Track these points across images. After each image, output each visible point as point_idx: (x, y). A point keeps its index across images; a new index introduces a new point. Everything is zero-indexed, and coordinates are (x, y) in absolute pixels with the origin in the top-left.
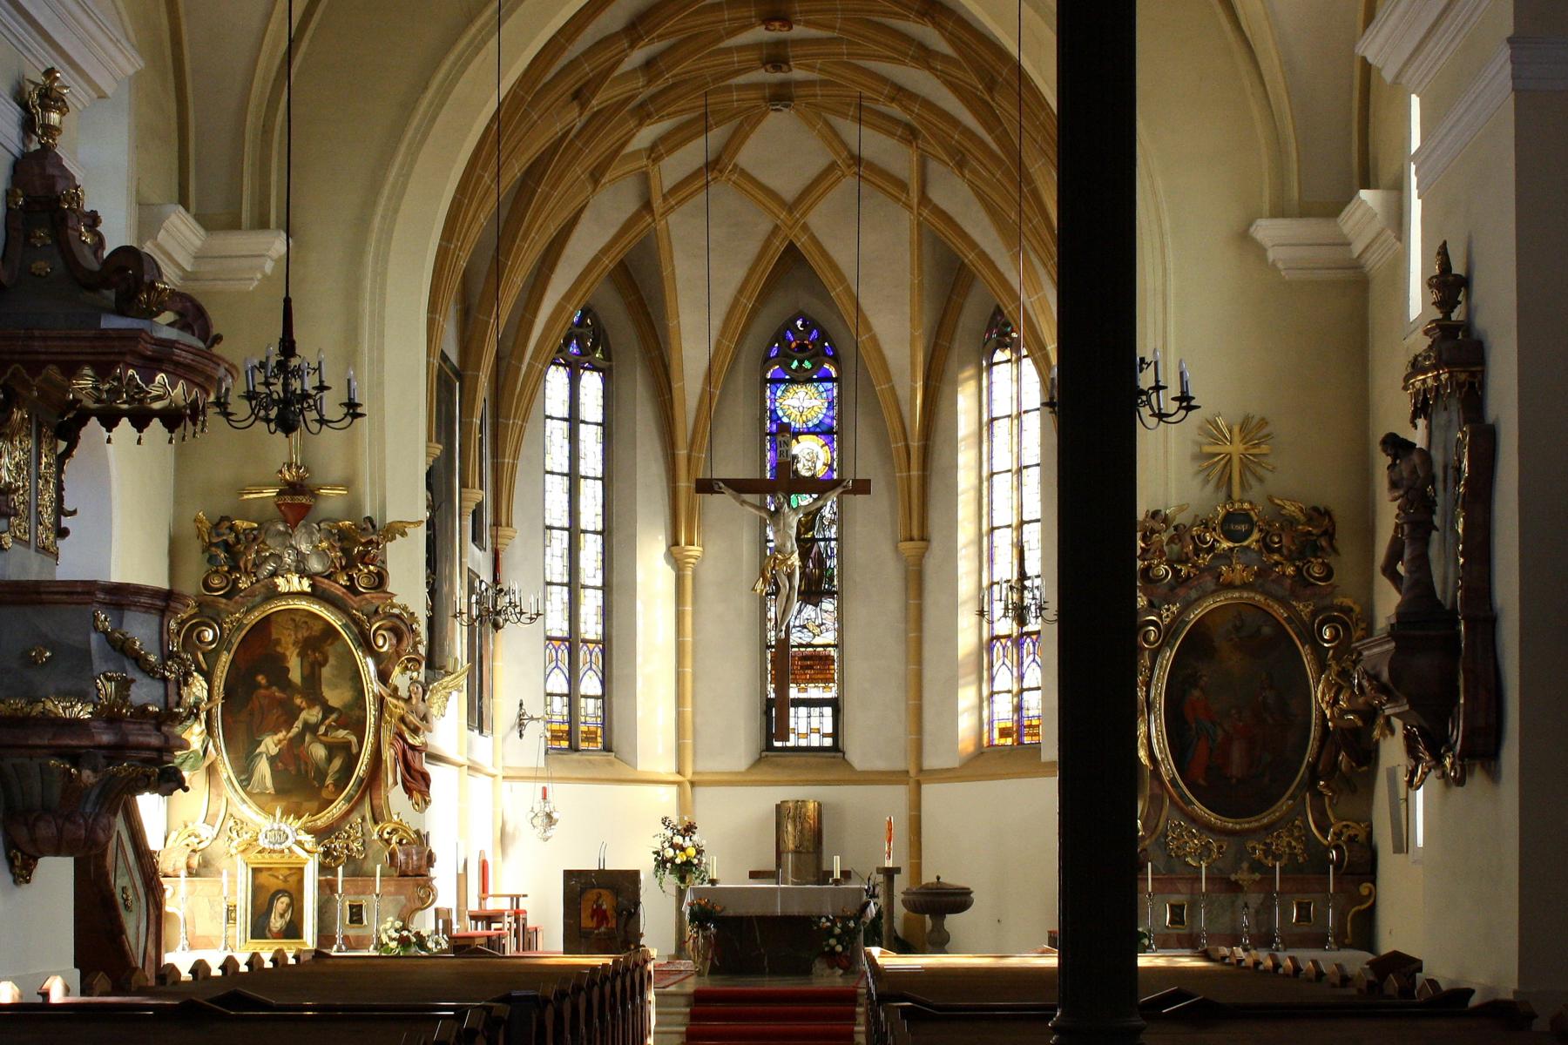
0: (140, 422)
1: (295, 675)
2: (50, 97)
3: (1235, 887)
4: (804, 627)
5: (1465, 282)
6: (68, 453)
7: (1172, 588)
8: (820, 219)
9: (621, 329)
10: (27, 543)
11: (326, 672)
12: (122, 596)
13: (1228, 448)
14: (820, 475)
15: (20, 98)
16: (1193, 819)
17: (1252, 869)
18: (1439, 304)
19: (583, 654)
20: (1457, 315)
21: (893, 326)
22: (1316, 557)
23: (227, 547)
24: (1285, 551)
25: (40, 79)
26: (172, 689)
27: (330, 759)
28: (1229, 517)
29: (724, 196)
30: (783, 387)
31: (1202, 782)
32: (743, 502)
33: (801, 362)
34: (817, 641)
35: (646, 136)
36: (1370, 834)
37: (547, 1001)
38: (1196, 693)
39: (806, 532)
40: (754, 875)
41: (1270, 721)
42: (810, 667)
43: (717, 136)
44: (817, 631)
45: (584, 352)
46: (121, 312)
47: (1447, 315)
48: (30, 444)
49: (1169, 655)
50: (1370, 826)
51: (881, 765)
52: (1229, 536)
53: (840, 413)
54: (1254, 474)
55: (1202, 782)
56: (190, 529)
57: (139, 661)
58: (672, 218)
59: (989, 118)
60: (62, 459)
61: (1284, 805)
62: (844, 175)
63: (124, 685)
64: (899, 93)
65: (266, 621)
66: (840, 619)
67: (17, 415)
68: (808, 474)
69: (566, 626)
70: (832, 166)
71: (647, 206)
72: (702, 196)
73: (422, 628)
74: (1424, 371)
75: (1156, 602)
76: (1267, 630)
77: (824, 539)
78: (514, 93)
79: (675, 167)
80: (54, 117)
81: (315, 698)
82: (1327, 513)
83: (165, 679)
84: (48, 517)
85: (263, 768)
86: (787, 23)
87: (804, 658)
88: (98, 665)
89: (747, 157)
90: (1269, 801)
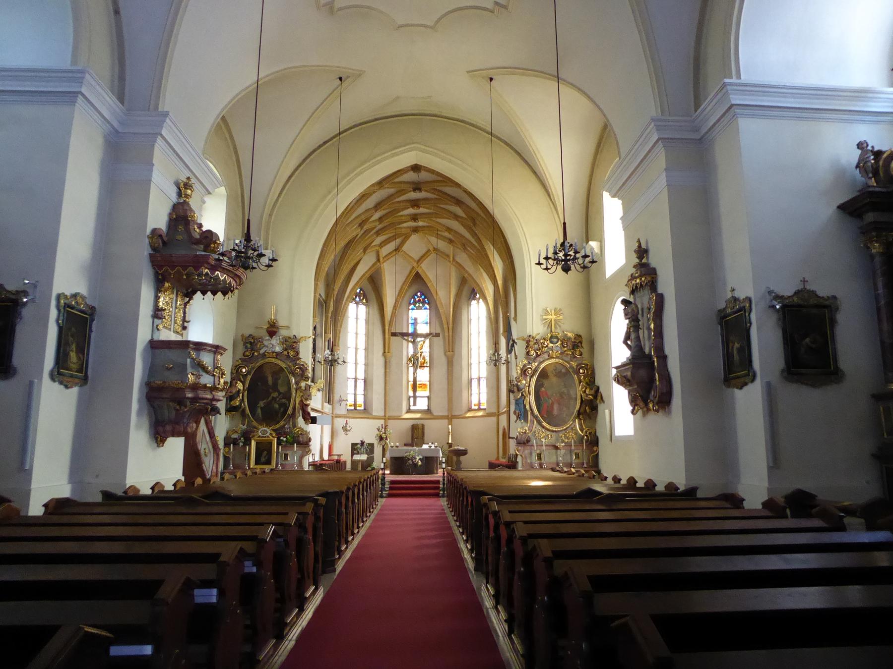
0: (214, 293)
1: (270, 382)
2: (187, 185)
3: (556, 448)
5: (646, 251)
6: (188, 302)
7: (535, 358)
9: (372, 292)
10: (170, 329)
11: (280, 382)
12: (199, 346)
13: (549, 317)
15: (177, 184)
16: (543, 427)
18: (638, 258)
19: (358, 382)
20: (644, 261)
21: (445, 294)
23: (251, 343)
25: (185, 180)
26: (217, 379)
27: (280, 408)
29: (399, 258)
35: (379, 240)
37: (342, 492)
38: (543, 389)
40: (405, 445)
43: (398, 241)
45: (361, 300)
46: (205, 251)
47: (641, 261)
48: (174, 296)
49: (535, 378)
51: (441, 414)
52: (551, 342)
56: (240, 338)
57: (204, 369)
59: (474, 235)
60: (185, 304)
63: (198, 376)
64: (449, 229)
65: (261, 367)
67: (167, 285)
70: (429, 250)
71: (378, 260)
72: (393, 259)
73: (310, 369)
74: (636, 278)
76: (563, 371)
78: (341, 216)
79: (385, 251)
80: (189, 192)
81: (275, 389)
82: (580, 336)
83: (214, 376)
84: (180, 322)
85: (259, 411)
86: (419, 207)
88: (189, 370)
89: (405, 248)
90: (565, 423)
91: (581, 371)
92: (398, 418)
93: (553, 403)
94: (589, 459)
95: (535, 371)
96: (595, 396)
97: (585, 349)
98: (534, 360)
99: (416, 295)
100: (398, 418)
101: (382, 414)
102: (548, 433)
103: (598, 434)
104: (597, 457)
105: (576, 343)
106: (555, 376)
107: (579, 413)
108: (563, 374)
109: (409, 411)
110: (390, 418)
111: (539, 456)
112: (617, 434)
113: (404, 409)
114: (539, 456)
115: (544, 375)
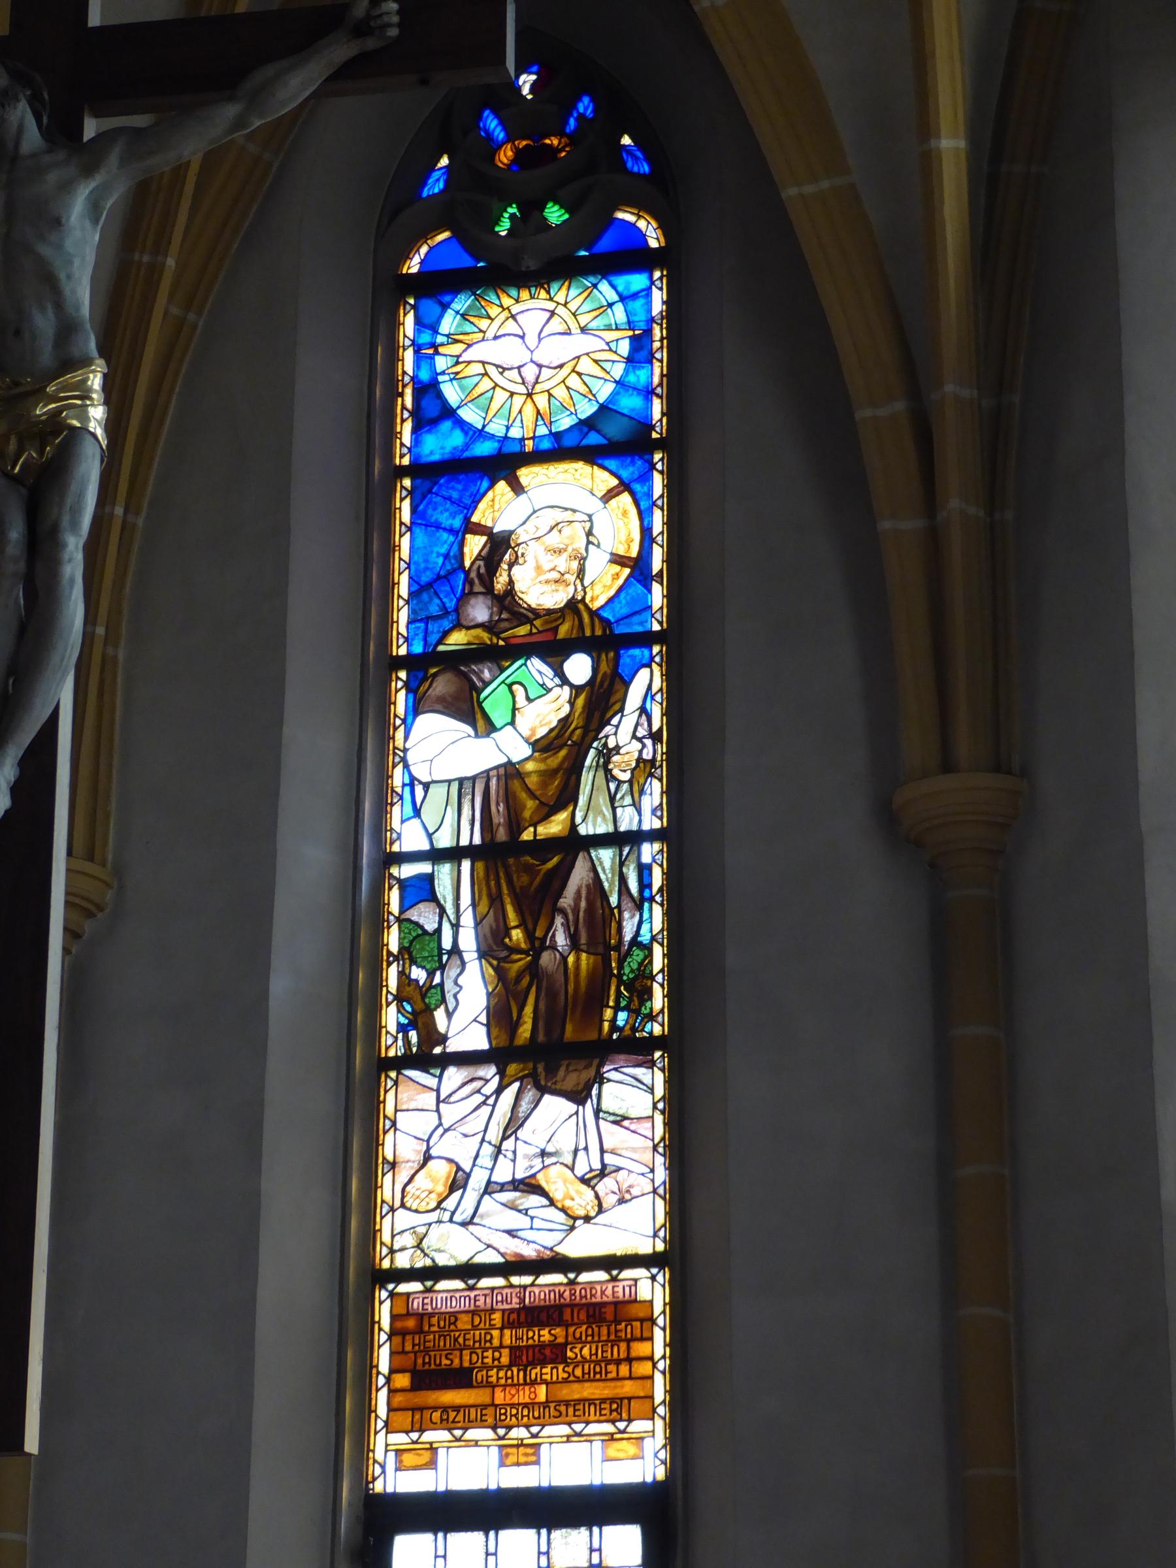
4: (529, 1186)
14: (598, 597)
30: (462, 302)
33: (532, 209)
34: (581, 1244)
39: (547, 812)
42: (555, 1354)
44: (582, 1201)
53: (675, 375)
66: (680, 1147)
68: (555, 599)
69: (639, 1375)
77: (616, 839)
87: (530, 1315)
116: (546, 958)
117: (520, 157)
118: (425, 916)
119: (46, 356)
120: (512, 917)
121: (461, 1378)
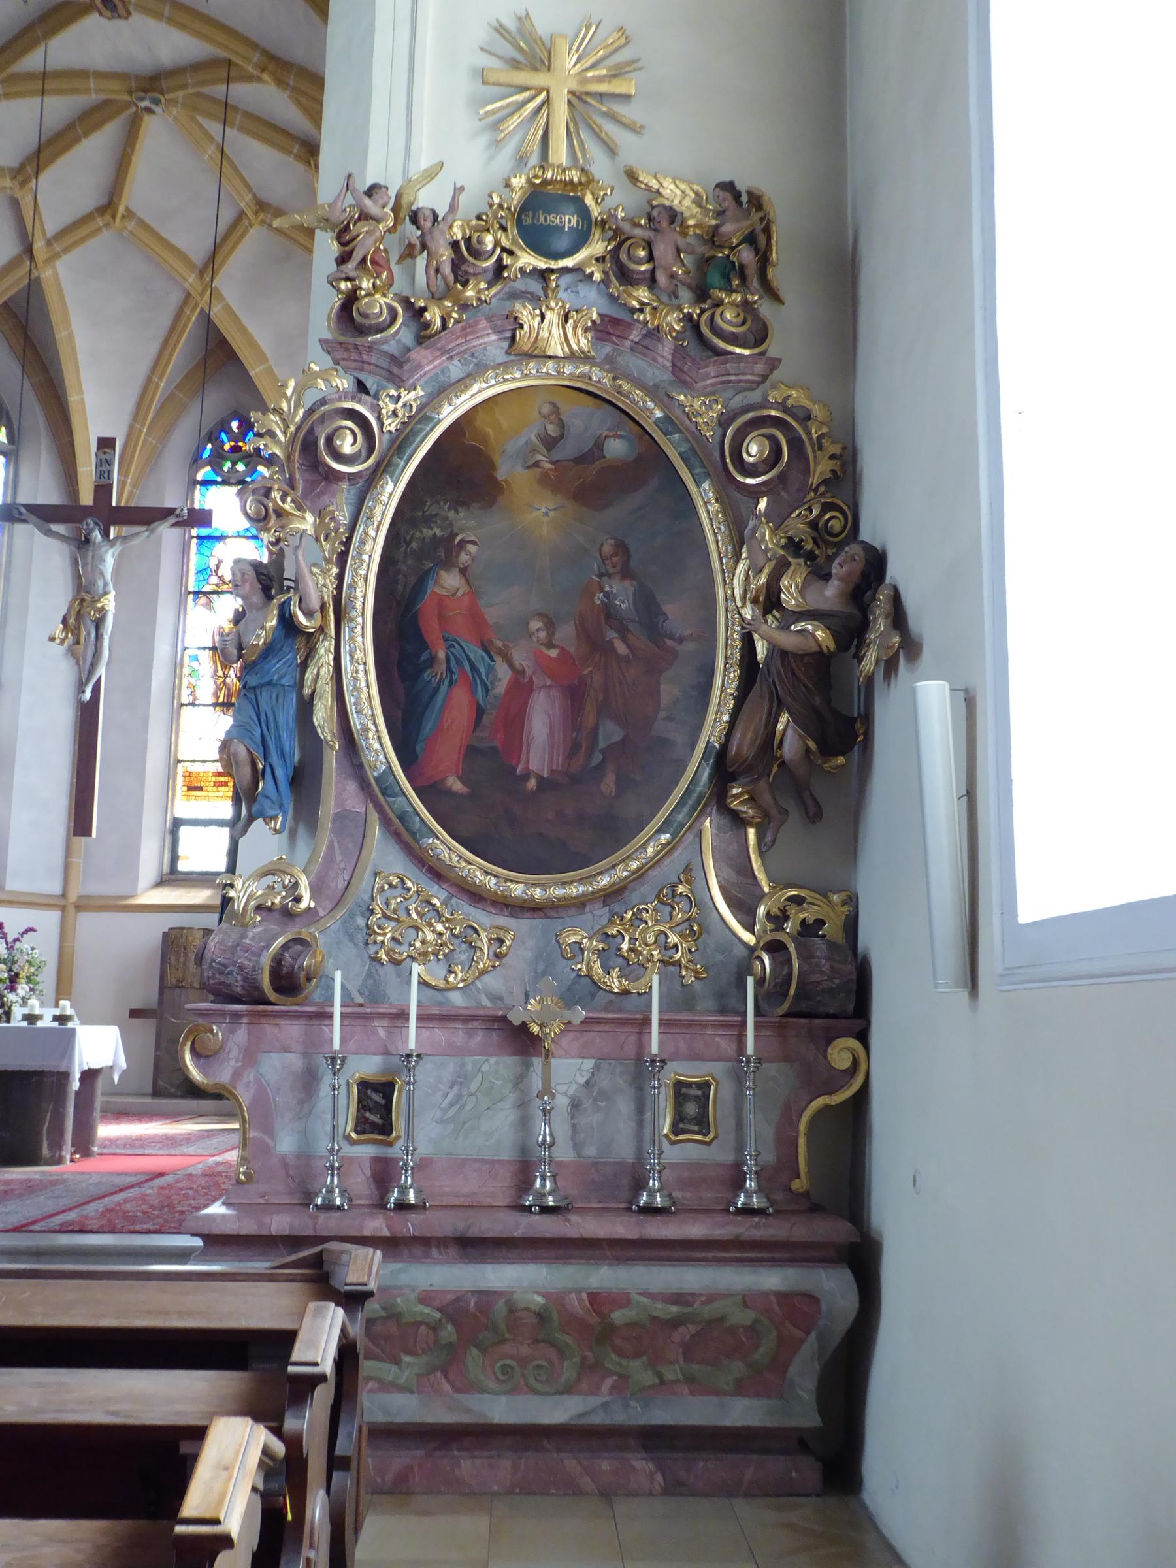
3: (522, 1040)
8: (231, 282)
16: (437, 873)
17: (569, 998)
22: (731, 291)
24: (661, 278)
28: (539, 198)
31: (455, 784)
32: (49, 533)
33: (234, 464)
36: (851, 926)
38: (450, 581)
41: (621, 648)
49: (391, 492)
50: (852, 901)
52: (537, 240)
54: (597, 135)
55: (455, 784)
58: (60, 264)
61: (651, 843)
62: (251, 225)
70: (241, 215)
71: (29, 251)
75: (370, 383)
82: (756, 201)
90: (613, 833)
91: (754, 450)
92: (118, 905)
93: (521, 689)
94: (786, 1143)
95: (401, 443)
96: (851, 632)
97: (792, 323)
98: (397, 371)
99: (224, 427)
100: (118, 905)
101: (56, 888)
102: (481, 917)
103: (869, 937)
104: (852, 1122)
105: (730, 251)
106: (552, 482)
107: (724, 769)
108: (620, 478)
109: (172, 877)
110: (85, 905)
111: (376, 1106)
112: (1029, 911)
113: (150, 862)
114: (376, 1106)
115: (459, 471)
116: (228, 680)
117: (232, 447)
118: (195, 665)
119: (101, 591)
120: (219, 667)
121: (200, 789)
